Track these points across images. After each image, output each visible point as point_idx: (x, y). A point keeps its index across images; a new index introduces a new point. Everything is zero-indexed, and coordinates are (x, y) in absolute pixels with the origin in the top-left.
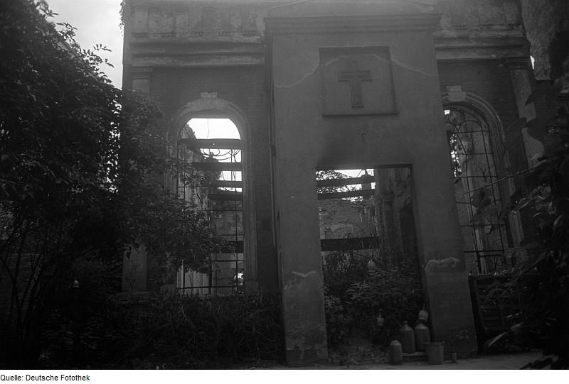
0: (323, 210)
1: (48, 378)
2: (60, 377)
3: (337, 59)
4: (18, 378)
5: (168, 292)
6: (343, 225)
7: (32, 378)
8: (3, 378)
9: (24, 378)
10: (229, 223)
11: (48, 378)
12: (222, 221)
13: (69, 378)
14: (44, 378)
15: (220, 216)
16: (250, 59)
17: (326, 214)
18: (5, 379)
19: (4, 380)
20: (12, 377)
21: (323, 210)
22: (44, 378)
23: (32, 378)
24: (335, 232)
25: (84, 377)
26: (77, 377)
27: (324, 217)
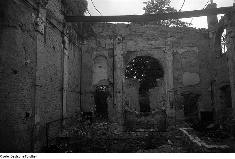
0: (171, 36)
1: (20, 157)
2: (25, 156)
3: (176, 20)
4: (8, 157)
5: (18, 129)
6: (189, 49)
7: (13, 157)
8: (1, 156)
9: (10, 157)
10: (92, 48)
11: (20, 157)
12: (86, 46)
13: (29, 157)
14: (18, 157)
15: (85, 42)
16: (151, 43)
17: (174, 39)
18: (2, 157)
19: (2, 157)
20: (5, 156)
21: (171, 36)
22: (18, 157)
23: (13, 157)
24: (182, 55)
25: (35, 156)
26: (32, 156)
27: (172, 41)
